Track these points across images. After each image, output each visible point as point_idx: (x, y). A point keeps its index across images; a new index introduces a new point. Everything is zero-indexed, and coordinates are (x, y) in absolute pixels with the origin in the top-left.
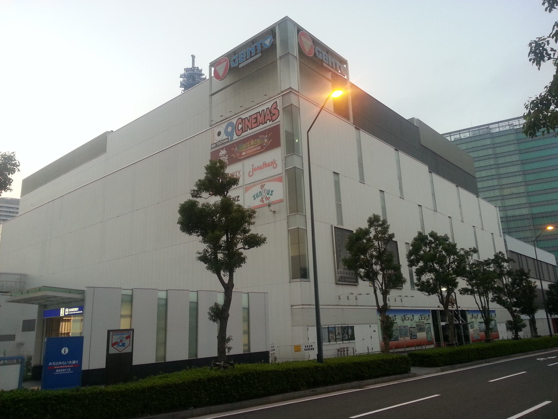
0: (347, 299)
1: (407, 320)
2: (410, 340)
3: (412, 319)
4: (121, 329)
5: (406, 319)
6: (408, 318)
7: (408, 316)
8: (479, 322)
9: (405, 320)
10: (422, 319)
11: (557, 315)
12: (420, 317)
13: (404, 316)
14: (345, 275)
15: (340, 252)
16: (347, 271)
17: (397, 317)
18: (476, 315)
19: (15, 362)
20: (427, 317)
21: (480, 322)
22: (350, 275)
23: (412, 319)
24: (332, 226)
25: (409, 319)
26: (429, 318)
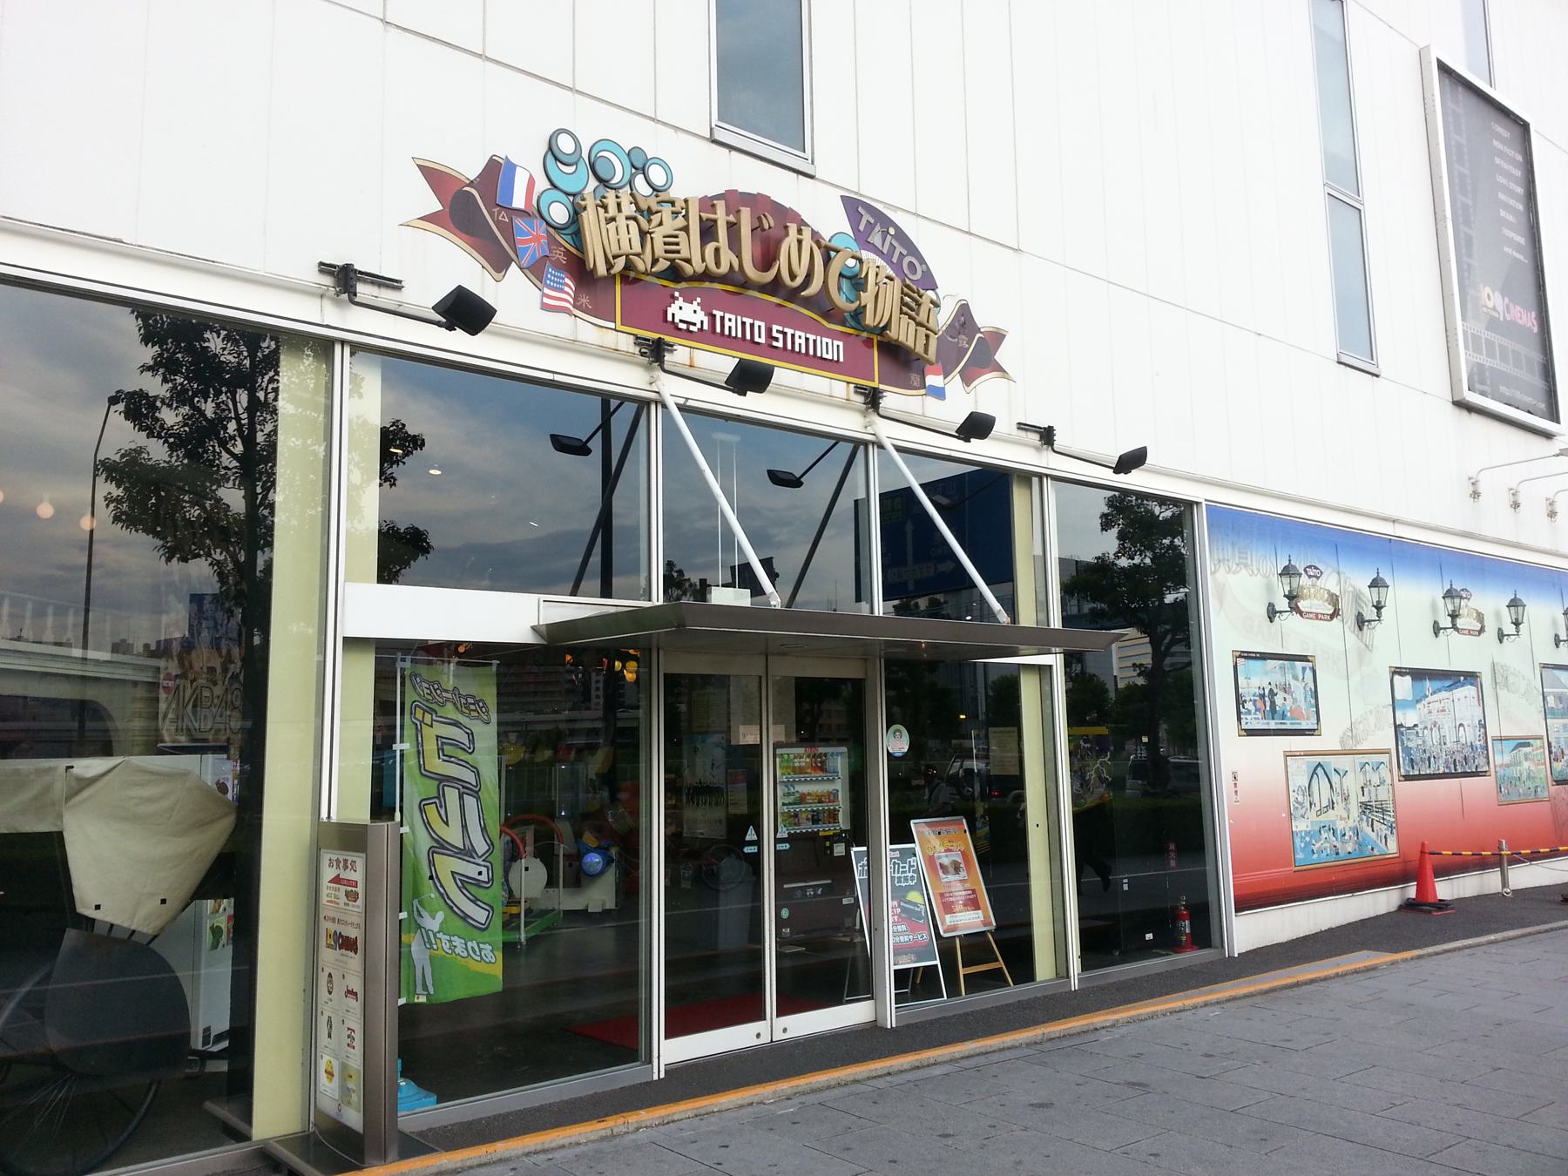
0: (1544, 511)
1: (1317, 617)
2: (1554, 789)
3: (1509, 629)
4: (583, 582)
5: (1302, 605)
6: (1480, 617)
7: (1330, 582)
8: (1398, 671)
9: (1454, 627)
10: (1460, 622)
11: (17, 516)
12: (1281, 588)
13: (1376, 583)
14: (1497, 364)
15: (1467, 223)
16: (1506, 342)
17: (1391, 597)
18: (1362, 581)
19: (247, 967)
20: (1498, 616)
21: (1418, 675)
22: (1504, 359)
23: (1370, 613)
24: (1422, 54)
25: (1482, 630)
26: (1517, 624)
